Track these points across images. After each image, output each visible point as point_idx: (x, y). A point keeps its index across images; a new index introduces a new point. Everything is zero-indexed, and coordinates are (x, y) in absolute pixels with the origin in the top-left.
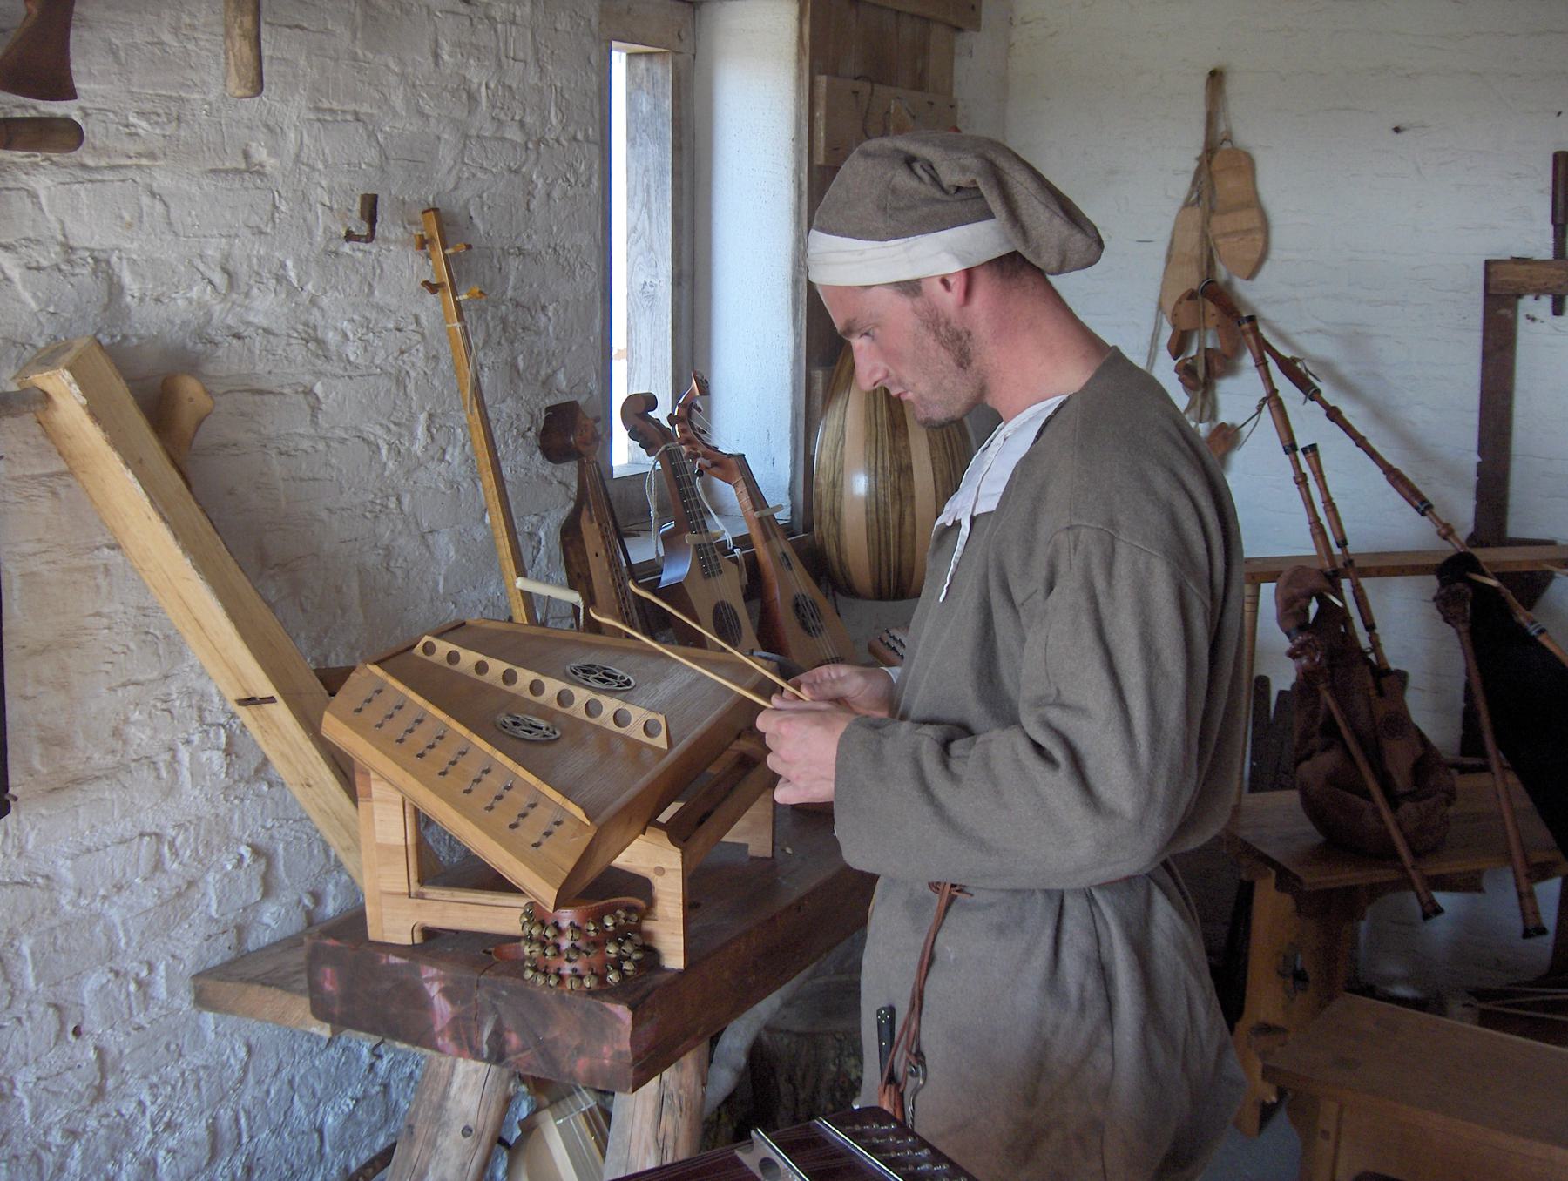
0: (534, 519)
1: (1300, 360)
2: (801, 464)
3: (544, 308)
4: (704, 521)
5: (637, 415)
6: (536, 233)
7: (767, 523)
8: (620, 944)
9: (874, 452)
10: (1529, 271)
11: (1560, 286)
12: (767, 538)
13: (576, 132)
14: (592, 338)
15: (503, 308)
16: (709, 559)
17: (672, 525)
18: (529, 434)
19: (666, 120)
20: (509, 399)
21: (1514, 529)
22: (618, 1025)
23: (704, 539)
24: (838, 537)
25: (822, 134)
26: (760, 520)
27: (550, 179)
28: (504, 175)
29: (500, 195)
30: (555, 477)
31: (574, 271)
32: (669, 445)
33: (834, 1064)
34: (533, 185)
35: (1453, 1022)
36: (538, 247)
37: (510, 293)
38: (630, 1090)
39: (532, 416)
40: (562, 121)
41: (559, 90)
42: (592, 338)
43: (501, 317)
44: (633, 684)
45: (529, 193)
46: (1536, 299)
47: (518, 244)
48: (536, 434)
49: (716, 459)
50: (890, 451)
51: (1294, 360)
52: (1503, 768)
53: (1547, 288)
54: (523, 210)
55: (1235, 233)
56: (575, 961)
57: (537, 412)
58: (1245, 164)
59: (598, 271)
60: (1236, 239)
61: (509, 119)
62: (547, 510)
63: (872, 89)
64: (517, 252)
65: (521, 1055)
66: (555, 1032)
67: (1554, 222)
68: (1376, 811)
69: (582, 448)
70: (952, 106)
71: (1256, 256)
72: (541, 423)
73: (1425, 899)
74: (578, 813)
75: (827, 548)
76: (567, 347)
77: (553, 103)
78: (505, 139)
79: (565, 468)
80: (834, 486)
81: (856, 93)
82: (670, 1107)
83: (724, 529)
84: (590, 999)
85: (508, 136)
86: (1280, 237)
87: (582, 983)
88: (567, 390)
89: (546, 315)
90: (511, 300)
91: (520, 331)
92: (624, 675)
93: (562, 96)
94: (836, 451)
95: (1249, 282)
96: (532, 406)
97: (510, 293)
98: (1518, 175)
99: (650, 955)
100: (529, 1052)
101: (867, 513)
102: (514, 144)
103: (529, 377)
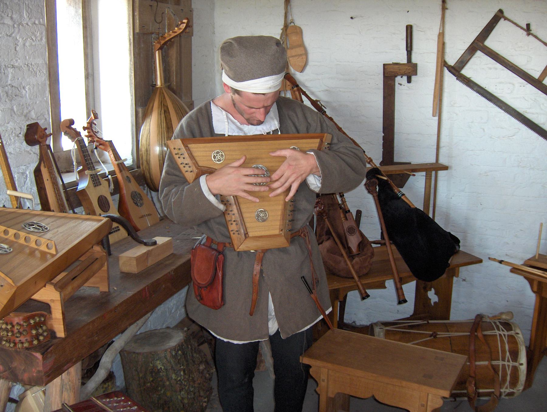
0: (24, 167)
1: (319, 101)
2: (135, 143)
3: (24, 88)
4: (93, 166)
5: (67, 127)
6: (19, 59)
7: (121, 166)
8: (37, 330)
9: (161, 138)
10: (398, 67)
11: (409, 73)
12: (121, 171)
13: (35, 21)
14: (45, 99)
15: (7, 88)
16: (95, 179)
17: (81, 168)
18: (20, 135)
19: (80, 17)
20: (11, 123)
21: (396, 160)
22: (38, 361)
23: (93, 172)
24: (149, 169)
25: (138, 21)
26: (118, 164)
27: (25, 38)
28: (4, 37)
29: (3, 45)
30: (32, 151)
31: (36, 73)
32: (79, 138)
33: (151, 363)
34: (18, 41)
35: (368, 336)
36: (21, 65)
37: (9, 82)
38: (44, 385)
39: (21, 128)
40: (29, 16)
41: (27, 5)
42: (45, 99)
43: (6, 91)
44: (48, 229)
45: (16, 44)
46: (401, 77)
47: (12, 64)
48: (23, 135)
49: (101, 143)
50: (167, 137)
51: (317, 101)
52: (391, 244)
53: (405, 74)
54: (13, 50)
55: (295, 56)
56: (20, 337)
57: (23, 127)
58: (299, 32)
59: (47, 73)
60: (296, 58)
61: (6, 16)
62: (29, 164)
63: (157, 4)
64: (12, 67)
65: (4, 373)
66: (15, 364)
67: (407, 50)
68: (345, 261)
69: (40, 140)
70: (191, 11)
71: (303, 64)
72: (25, 131)
73: (363, 292)
74: (10, 281)
75: (146, 174)
76: (35, 102)
77: (25, 10)
78: (4, 23)
79: (36, 147)
80: (147, 151)
81: (151, 6)
82: (66, 389)
83: (104, 169)
84: (27, 351)
85: (6, 22)
86: (311, 57)
87: (23, 345)
88: (36, 118)
89: (25, 90)
90: (10, 85)
91: (14, 96)
92: (45, 225)
93: (28, 7)
94: (147, 138)
95: (301, 73)
96: (21, 125)
97: (9, 82)
98: (394, 34)
99: (52, 334)
100: (6, 372)
101: (159, 160)
102: (8, 26)
103: (19, 113)
